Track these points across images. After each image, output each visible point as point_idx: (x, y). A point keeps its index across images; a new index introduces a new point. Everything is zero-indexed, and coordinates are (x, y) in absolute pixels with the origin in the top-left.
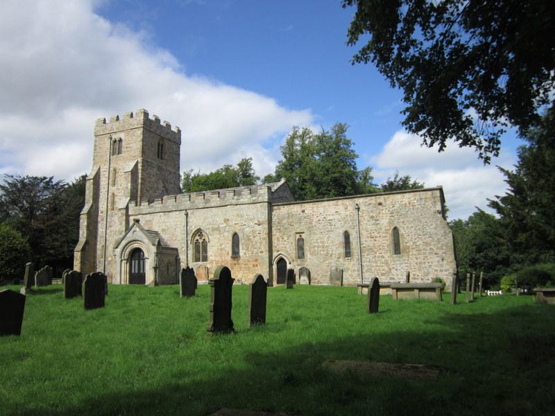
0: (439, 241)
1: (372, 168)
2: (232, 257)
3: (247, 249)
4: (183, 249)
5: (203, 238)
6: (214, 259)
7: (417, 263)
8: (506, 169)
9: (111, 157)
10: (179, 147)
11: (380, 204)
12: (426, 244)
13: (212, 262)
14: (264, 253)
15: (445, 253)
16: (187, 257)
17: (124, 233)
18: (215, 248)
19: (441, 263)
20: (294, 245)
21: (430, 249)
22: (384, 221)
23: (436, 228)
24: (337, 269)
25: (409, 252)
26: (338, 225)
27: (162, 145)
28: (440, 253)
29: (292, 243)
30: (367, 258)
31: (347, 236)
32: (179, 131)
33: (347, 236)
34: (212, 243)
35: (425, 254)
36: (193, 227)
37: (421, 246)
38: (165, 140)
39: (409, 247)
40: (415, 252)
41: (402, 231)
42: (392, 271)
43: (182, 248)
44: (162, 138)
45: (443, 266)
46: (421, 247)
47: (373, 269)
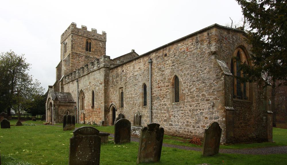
0: (211, 87)
7: (190, 111)
10: (105, 44)
11: (166, 55)
12: (199, 90)
14: (103, 103)
15: (216, 99)
19: (211, 110)
20: (118, 97)
21: (203, 95)
22: (167, 72)
23: (209, 72)
24: (137, 115)
25: (185, 99)
26: (140, 79)
27: (90, 43)
28: (211, 99)
29: (117, 96)
30: (156, 104)
31: (145, 86)
32: (104, 34)
33: (145, 86)
35: (197, 100)
37: (195, 92)
38: (91, 40)
39: (185, 94)
40: (190, 100)
41: (180, 79)
42: (172, 117)
45: (213, 113)
46: (195, 94)
47: (159, 115)
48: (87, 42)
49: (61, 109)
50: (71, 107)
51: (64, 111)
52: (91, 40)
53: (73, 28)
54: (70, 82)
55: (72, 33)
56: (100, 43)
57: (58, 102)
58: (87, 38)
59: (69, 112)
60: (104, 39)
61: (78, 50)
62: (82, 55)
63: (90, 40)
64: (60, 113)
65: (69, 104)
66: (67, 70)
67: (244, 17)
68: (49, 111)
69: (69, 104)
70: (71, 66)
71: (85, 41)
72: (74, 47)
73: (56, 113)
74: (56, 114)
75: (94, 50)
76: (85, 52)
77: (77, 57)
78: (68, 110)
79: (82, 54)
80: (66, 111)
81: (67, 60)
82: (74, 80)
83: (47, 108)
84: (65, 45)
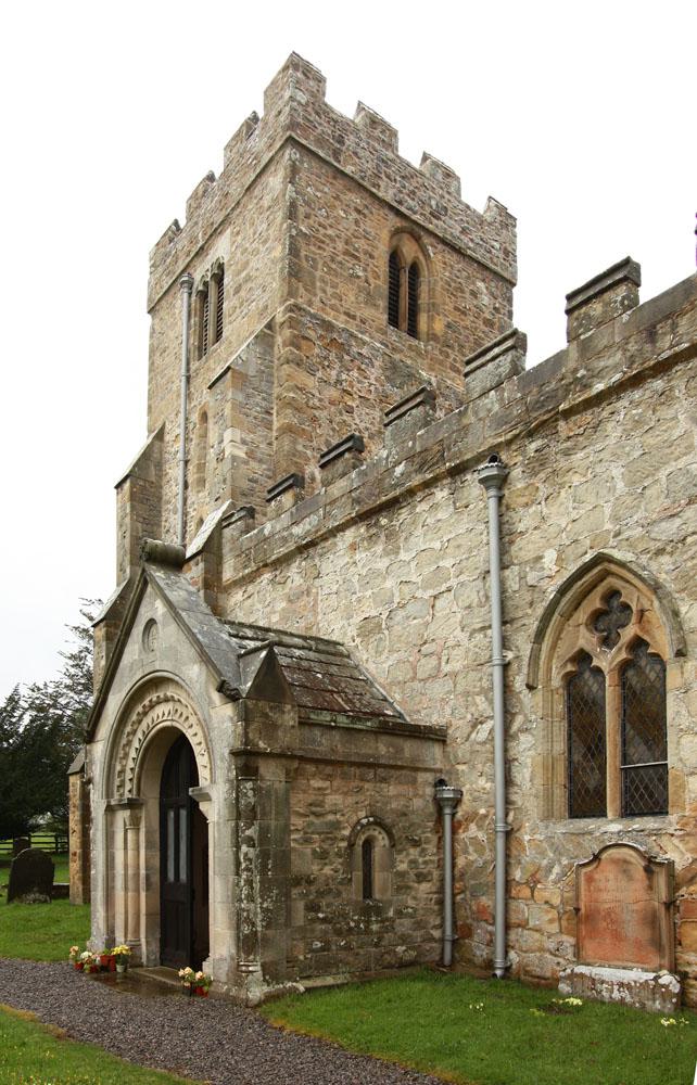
4: (482, 733)
5: (629, 633)
9: (194, 365)
10: (510, 300)
16: (508, 782)
27: (414, 270)
36: (550, 557)
43: (476, 723)
44: (414, 231)
48: (394, 258)
49: (315, 807)
50: (401, 789)
51: (337, 826)
52: (426, 240)
53: (302, 98)
54: (342, 528)
55: (290, 139)
56: (480, 284)
57: (289, 717)
58: (398, 223)
59: (382, 840)
60: (501, 255)
61: (335, 296)
62: (364, 351)
63: (417, 239)
64: (304, 861)
65: (383, 749)
66: (253, 464)
67: (206, 682)
68: (135, 823)
69: (382, 748)
70: (288, 430)
71: (385, 235)
72: (304, 264)
73: (264, 855)
74: (263, 870)
75: (439, 326)
76: (385, 333)
77: (332, 356)
78: (379, 823)
79: (364, 343)
80: (358, 828)
81: (252, 372)
82: (411, 492)
83: (109, 795)
84: (204, 295)
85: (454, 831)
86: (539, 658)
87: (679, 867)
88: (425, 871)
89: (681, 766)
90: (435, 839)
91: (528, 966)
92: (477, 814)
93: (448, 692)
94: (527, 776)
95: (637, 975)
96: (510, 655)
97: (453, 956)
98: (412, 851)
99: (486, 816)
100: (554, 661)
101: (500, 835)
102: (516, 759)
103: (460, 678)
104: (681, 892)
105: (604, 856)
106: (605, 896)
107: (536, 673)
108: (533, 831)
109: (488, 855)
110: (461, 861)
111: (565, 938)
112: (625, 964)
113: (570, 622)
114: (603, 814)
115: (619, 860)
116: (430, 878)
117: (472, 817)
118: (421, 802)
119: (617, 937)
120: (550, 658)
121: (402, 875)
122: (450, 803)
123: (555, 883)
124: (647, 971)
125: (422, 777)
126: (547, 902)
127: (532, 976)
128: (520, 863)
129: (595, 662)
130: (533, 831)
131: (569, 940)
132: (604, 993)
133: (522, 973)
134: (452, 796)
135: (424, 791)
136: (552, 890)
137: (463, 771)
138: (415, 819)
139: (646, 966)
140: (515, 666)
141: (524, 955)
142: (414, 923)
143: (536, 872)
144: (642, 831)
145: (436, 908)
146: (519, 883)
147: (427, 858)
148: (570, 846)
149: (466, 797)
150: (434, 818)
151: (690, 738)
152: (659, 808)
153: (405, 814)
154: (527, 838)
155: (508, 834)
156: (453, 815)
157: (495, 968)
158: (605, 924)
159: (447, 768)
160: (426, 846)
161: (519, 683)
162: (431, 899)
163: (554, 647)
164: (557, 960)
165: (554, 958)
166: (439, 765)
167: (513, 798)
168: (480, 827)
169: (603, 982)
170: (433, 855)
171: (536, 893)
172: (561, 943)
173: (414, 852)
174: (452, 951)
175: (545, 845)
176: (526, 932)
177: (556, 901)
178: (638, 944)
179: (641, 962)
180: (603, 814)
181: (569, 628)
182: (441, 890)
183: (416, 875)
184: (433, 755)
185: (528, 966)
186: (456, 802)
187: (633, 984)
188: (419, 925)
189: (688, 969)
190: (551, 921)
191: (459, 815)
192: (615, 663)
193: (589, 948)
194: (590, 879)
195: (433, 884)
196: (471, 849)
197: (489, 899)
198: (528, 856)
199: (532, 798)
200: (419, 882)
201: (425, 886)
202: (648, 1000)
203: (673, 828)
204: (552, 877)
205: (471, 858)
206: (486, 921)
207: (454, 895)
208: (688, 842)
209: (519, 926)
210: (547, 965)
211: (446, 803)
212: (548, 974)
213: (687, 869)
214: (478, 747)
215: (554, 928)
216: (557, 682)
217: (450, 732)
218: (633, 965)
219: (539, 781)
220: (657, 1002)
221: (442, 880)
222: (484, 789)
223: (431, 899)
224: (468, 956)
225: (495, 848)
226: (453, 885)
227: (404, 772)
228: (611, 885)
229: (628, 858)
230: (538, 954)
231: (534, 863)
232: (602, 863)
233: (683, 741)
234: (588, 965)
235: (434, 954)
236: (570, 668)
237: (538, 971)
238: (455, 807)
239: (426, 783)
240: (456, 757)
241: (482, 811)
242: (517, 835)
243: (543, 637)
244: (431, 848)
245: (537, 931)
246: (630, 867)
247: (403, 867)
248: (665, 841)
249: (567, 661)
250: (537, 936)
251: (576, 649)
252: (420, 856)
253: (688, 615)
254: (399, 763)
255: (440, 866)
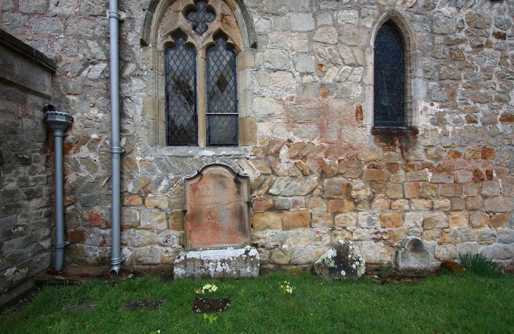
1: (240, 206)
2: (374, 132)
3: (449, 101)
6: (283, 134)
8: (306, 30)
13: (270, 153)
17: (172, 114)
18: (287, 83)
34: (266, 53)
85: (65, 151)
86: (151, 24)
87: (252, 179)
88: (35, 188)
89: (254, 115)
90: (43, 158)
91: (140, 257)
92: (89, 138)
93: (57, 31)
94: (139, 111)
95: (231, 253)
96: (123, 16)
97: (64, 261)
98: (21, 169)
99: (98, 140)
100: (159, 31)
101: (115, 156)
102: (129, 97)
103: (71, 22)
104: (254, 194)
105: (204, 172)
106: (207, 200)
107: (149, 33)
108: (144, 153)
109: (101, 172)
110: (72, 178)
111: (172, 232)
112: (222, 245)
113: (171, 7)
114: (196, 143)
115: (216, 175)
116: (39, 195)
117: (84, 140)
118: (31, 123)
119: (216, 228)
120: (158, 28)
121: (11, 194)
122: (62, 127)
123: (163, 192)
124: (236, 248)
125: (32, 99)
126: (156, 207)
127: (143, 265)
128: (132, 178)
129: (190, 40)
130: (144, 153)
131: (175, 234)
132: (210, 269)
133: (134, 263)
134: (64, 120)
135: (34, 113)
136: (161, 198)
137: (73, 101)
138: (23, 137)
139: (236, 245)
140: (128, 25)
141: (135, 249)
142: (26, 240)
143: (147, 185)
144: (229, 156)
145: (45, 220)
146: (131, 194)
147: (37, 175)
148: (176, 165)
149: (77, 124)
150: (43, 139)
151: (260, 99)
152: (233, 142)
153: (14, 133)
154: (138, 159)
155: (122, 155)
156: (64, 138)
157: (112, 266)
158: (207, 219)
159: (56, 96)
160: (35, 164)
161: (132, 39)
162: (41, 213)
163: (162, 16)
164: (164, 249)
165: (163, 248)
166: (47, 92)
167: (126, 127)
168: (92, 149)
169: (209, 262)
170: (43, 172)
171: (147, 201)
172: (168, 236)
173: (23, 171)
174: (64, 256)
175: (154, 164)
176: (137, 231)
177: (164, 205)
178: (231, 232)
179: (232, 242)
180: (196, 143)
181: (171, 11)
182: (51, 203)
183: (26, 193)
184: (43, 82)
185: (140, 257)
186: (68, 126)
187: (231, 259)
188: (31, 240)
189: (257, 242)
190: (160, 221)
191: (70, 138)
192: (205, 43)
193: (195, 238)
194: (195, 189)
195: (44, 200)
196: (82, 167)
197: (102, 208)
198: (140, 172)
199: (143, 129)
200: (29, 199)
201: (35, 203)
202: (242, 267)
203: (249, 154)
204: (161, 188)
205: (82, 175)
206: (99, 226)
207: (65, 207)
208: (257, 163)
209: (131, 227)
210: (160, 255)
211: (57, 126)
212: (158, 261)
213: (258, 180)
214: (90, 83)
215: (164, 225)
216: (160, 47)
217: (60, 65)
218: (227, 245)
219: (149, 116)
220: (248, 268)
221: (52, 193)
222: (97, 118)
223: (41, 213)
224: (79, 257)
225: (111, 164)
226: (64, 198)
227: (13, 89)
228: (211, 192)
229: (223, 174)
230: (149, 247)
231: (144, 178)
232: (204, 179)
233: (255, 100)
234: (195, 250)
235: (44, 263)
236: (170, 39)
237: (150, 260)
238: (65, 131)
239: (36, 106)
240: (66, 88)
241: (94, 136)
242: (129, 156)
243: (155, 9)
244: (41, 167)
245: (148, 229)
246: (226, 180)
247: (12, 186)
248: (243, 162)
249: (168, 34)
250: (148, 233)
251: (176, 27)
252: (30, 174)
253: (257, 24)
254: (8, 78)
255: (51, 181)
